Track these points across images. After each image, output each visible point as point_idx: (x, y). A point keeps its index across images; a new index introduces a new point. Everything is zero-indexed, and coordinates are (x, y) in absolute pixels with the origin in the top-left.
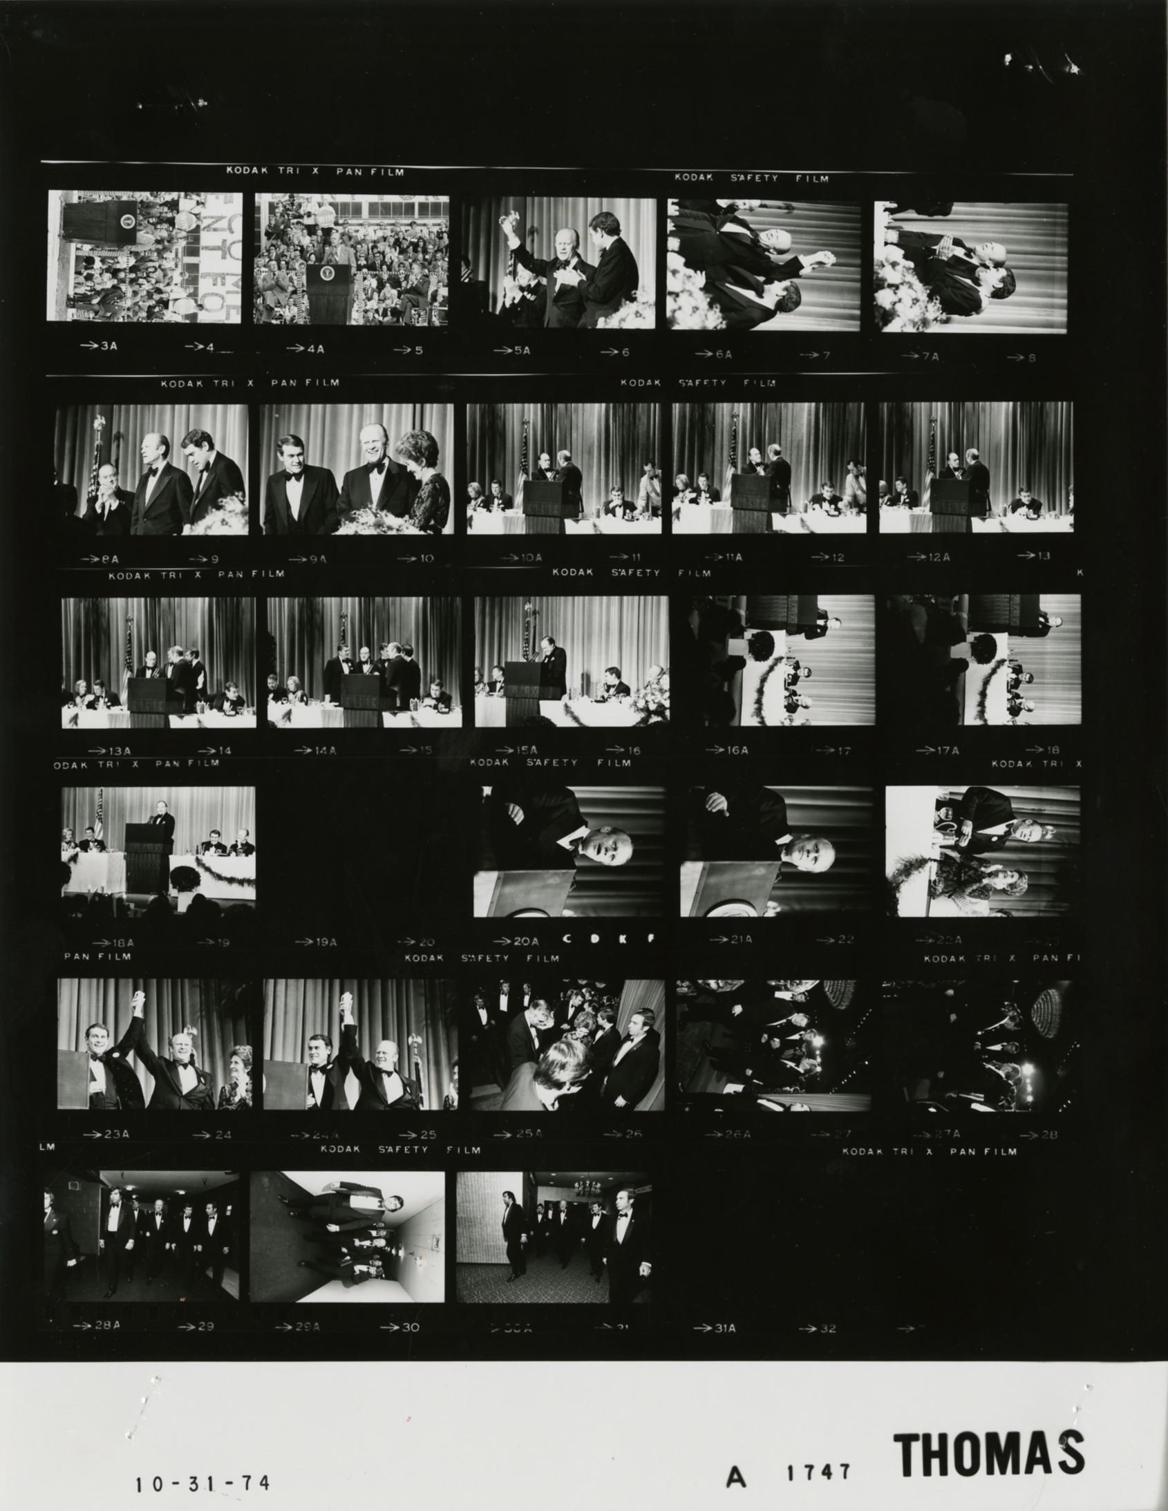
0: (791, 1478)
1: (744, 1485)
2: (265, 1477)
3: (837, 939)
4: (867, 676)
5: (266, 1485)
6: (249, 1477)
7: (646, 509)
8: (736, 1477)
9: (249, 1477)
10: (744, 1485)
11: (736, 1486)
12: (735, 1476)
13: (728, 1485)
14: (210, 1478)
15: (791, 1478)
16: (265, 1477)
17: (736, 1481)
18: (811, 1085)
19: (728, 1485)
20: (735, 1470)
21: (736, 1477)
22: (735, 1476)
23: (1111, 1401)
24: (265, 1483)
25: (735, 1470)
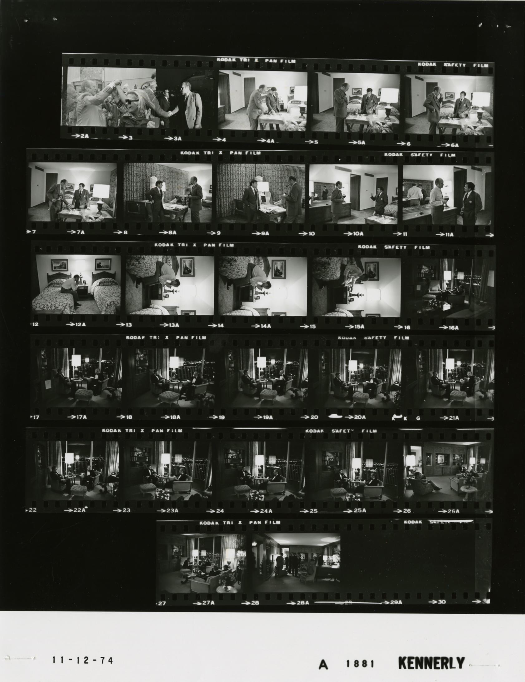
0: (54, 662)
1: (327, 668)
2: (111, 658)
3: (29, 510)
4: (450, 180)
5: (111, 662)
6: (104, 658)
7: (125, 123)
8: (323, 664)
9: (104, 658)
10: (327, 668)
11: (323, 669)
12: (323, 664)
13: (320, 668)
14: (54, 657)
15: (54, 662)
16: (111, 658)
17: (323, 666)
18: (372, 472)
19: (320, 668)
20: (323, 661)
21: (323, 664)
22: (323, 664)
23: (480, 639)
24: (111, 661)
25: (323, 661)
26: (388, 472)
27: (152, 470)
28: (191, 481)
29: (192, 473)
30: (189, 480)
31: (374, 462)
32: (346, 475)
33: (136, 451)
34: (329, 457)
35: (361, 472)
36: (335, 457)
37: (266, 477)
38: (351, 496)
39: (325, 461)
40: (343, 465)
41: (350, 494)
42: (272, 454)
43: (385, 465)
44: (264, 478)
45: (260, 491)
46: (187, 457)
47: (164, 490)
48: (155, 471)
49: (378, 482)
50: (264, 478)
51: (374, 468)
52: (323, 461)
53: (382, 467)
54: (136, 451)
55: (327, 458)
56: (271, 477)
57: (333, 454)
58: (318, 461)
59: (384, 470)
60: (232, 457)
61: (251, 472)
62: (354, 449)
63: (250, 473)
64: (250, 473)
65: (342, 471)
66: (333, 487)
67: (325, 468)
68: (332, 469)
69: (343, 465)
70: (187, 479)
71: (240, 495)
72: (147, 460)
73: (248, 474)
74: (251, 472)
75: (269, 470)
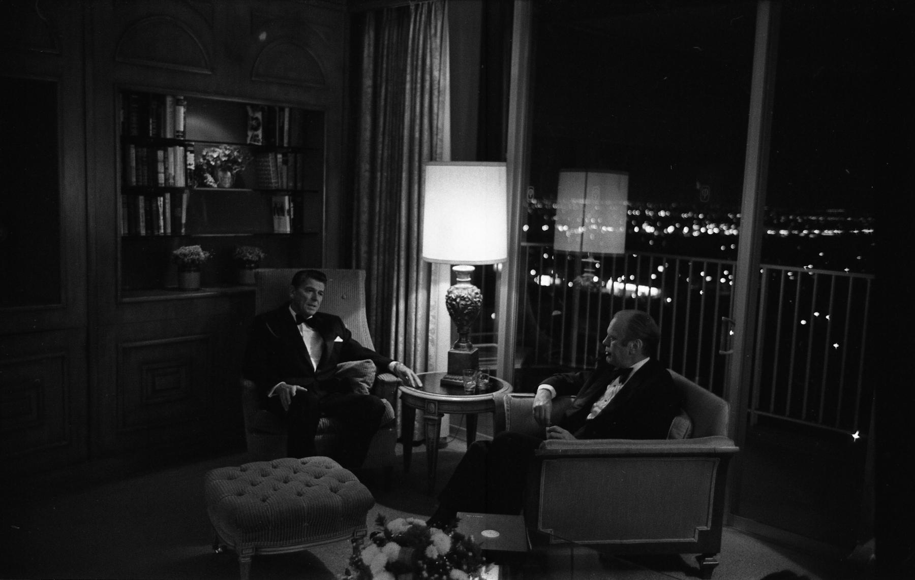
18: (623, 301)
26: (776, 302)
27: (327, 325)
28: (727, 445)
29: (735, 354)
30: (704, 427)
31: (635, 197)
32: (361, 332)
33: (179, 141)
34: (196, 149)
35: (505, 294)
36: (257, 153)
37: (525, 383)
38: (415, 541)
39: (153, 190)
40: (329, 235)
41: (399, 524)
42: (594, 159)
43: (742, 231)
44: (505, 394)
45: (467, 522)
46: (683, 202)
47: (446, 522)
48: (361, 332)
49: (680, 401)
50: (505, 394)
51: (635, 258)
52: (130, 193)
53: (718, 251)
54: (179, 141)
55: (176, 167)
56: (576, 386)
57: (234, 120)
58: (84, 190)
59: (738, 280)
60: (195, 175)
61: (381, 329)
62: (442, 76)
63: (365, 338)
64: (365, 338)
65: (318, 294)
66: (232, 448)
67: (147, 261)
68: (225, 267)
69: (329, 235)
70: (683, 423)
71: (259, 561)
72: (285, 225)
73: (352, 350)
74: (381, 329)
75: (543, 310)
